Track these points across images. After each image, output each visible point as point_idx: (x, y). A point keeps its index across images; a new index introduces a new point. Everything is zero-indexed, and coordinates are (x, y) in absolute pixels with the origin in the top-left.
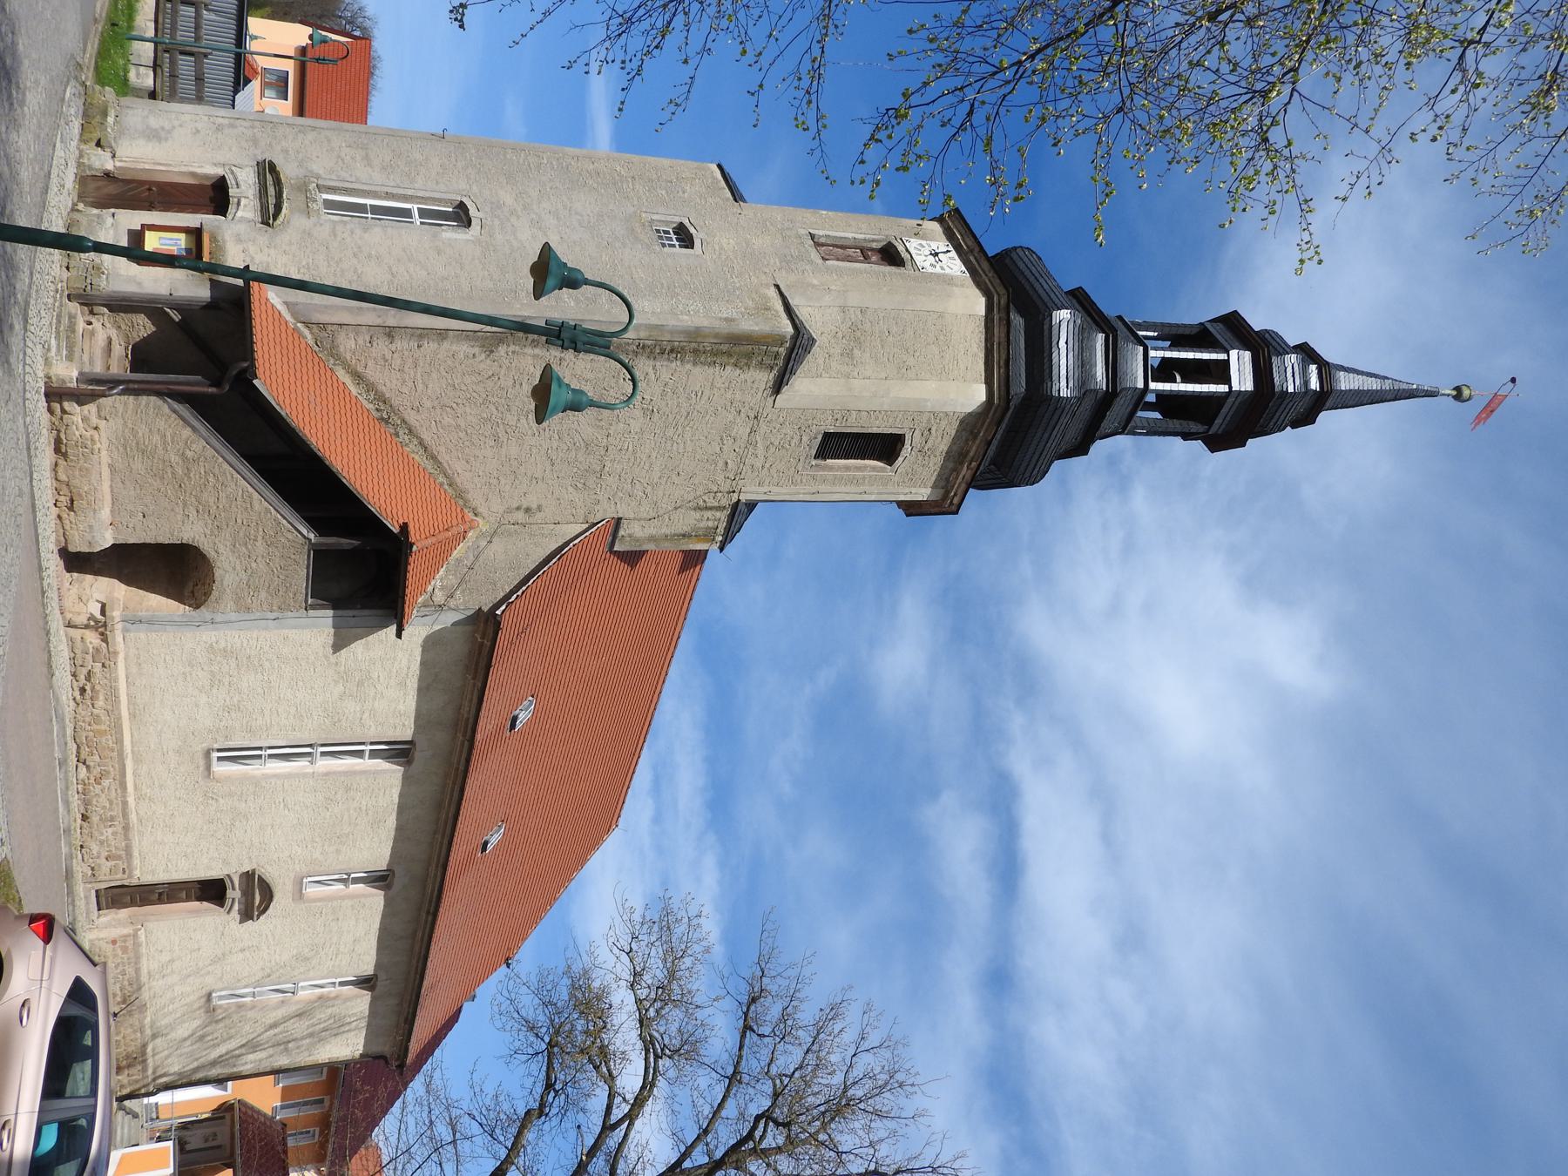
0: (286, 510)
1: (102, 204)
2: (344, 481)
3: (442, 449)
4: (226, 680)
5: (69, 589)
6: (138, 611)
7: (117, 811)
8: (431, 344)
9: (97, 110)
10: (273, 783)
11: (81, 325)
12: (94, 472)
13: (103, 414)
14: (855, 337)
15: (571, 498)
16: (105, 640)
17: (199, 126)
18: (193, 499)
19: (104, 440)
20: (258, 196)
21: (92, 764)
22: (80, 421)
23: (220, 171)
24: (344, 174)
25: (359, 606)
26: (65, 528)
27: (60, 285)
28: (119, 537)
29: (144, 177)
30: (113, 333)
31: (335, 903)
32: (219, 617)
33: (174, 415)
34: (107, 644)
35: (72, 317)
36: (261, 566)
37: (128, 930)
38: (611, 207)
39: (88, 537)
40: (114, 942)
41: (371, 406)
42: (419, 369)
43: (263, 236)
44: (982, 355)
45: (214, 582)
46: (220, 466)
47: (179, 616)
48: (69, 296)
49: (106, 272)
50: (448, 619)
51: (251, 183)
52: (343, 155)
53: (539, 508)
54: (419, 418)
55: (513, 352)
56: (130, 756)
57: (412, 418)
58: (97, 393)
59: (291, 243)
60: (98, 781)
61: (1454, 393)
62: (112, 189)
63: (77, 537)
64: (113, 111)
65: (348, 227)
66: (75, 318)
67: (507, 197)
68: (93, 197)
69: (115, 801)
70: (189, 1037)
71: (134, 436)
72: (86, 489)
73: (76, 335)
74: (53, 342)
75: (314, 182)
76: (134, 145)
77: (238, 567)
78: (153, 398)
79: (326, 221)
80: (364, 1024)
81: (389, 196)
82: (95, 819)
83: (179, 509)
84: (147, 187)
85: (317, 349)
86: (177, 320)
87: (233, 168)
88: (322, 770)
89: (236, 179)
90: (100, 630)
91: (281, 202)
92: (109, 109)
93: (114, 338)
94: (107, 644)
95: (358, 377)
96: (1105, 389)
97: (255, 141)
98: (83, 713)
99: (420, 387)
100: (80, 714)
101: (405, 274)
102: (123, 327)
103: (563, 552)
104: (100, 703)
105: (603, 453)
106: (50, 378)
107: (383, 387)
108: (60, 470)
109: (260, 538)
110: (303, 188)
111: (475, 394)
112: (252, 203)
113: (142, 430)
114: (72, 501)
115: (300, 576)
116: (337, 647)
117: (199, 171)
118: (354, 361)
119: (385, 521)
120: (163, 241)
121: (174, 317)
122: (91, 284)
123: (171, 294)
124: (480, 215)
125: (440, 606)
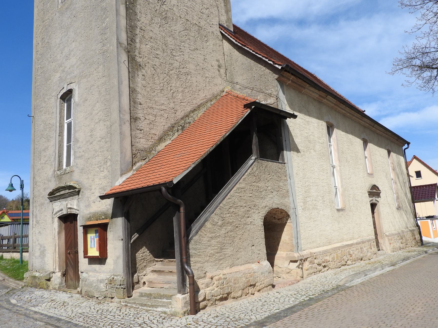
0: (242, 170)
1: (78, 278)
2: (227, 134)
3: (194, 102)
4: (315, 202)
5: (283, 278)
6: (293, 245)
7: (359, 247)
8: (139, 97)
9: (34, 281)
10: (344, 183)
11: (145, 289)
12: (236, 276)
13: (203, 275)
15: (211, 45)
16: (306, 259)
17: (37, 232)
18: (243, 220)
19: (218, 272)
20: (65, 199)
21: (347, 259)
22: (209, 288)
23: (56, 219)
24: (52, 159)
25: (281, 138)
26: (263, 287)
27: (122, 304)
28: (264, 258)
29: (64, 257)
30: (149, 269)
31: (373, 162)
32: (292, 206)
33: (199, 233)
34: (308, 258)
35: (141, 295)
36: (269, 184)
37: (386, 239)
38: (57, 25)
39: (267, 274)
40: (390, 244)
41: (176, 134)
42: (154, 106)
43: (85, 193)
45: (278, 208)
46: (225, 205)
47: (293, 225)
48: (128, 297)
49: (113, 276)
50: (281, 95)
51: (60, 204)
52: (44, 162)
53: (218, 61)
54: (180, 111)
55: (139, 54)
56: (342, 243)
57: (180, 114)
58: (191, 282)
59: (88, 178)
60: (351, 255)
62: (71, 273)
63: (267, 280)
64: (34, 273)
65: (77, 150)
66: (142, 293)
68: (76, 281)
69: (356, 248)
70: (406, 216)
71: (214, 255)
72: (244, 279)
73: (152, 292)
74: (160, 309)
75: (57, 172)
76: (48, 263)
77: (271, 196)
78: (191, 246)
79: (75, 162)
80: (398, 155)
81: (61, 134)
82: (362, 255)
83: (248, 227)
84: (68, 255)
85: (147, 160)
86: (138, 235)
87: (54, 213)
88: (338, 162)
89: (59, 211)
90: (303, 262)
91: (67, 187)
92: (33, 275)
93: (151, 269)
94: (308, 258)
95: (161, 139)
97: (42, 204)
98: (332, 265)
99: (163, 107)
100: (332, 266)
101: (99, 114)
102: (145, 264)
103: (240, 45)
104: (328, 258)
105: (189, 23)
106: (185, 313)
107: (166, 126)
108: (236, 295)
109: (257, 184)
110: (59, 177)
111: (165, 80)
112: (70, 202)
113: (210, 251)
114: (251, 285)
115: (272, 165)
116: (298, 151)
117: (57, 230)
118: (152, 140)
119: (245, 116)
120: (93, 245)
121: (136, 237)
122: (120, 285)
123: (122, 240)
124: (65, 86)
125: (277, 99)
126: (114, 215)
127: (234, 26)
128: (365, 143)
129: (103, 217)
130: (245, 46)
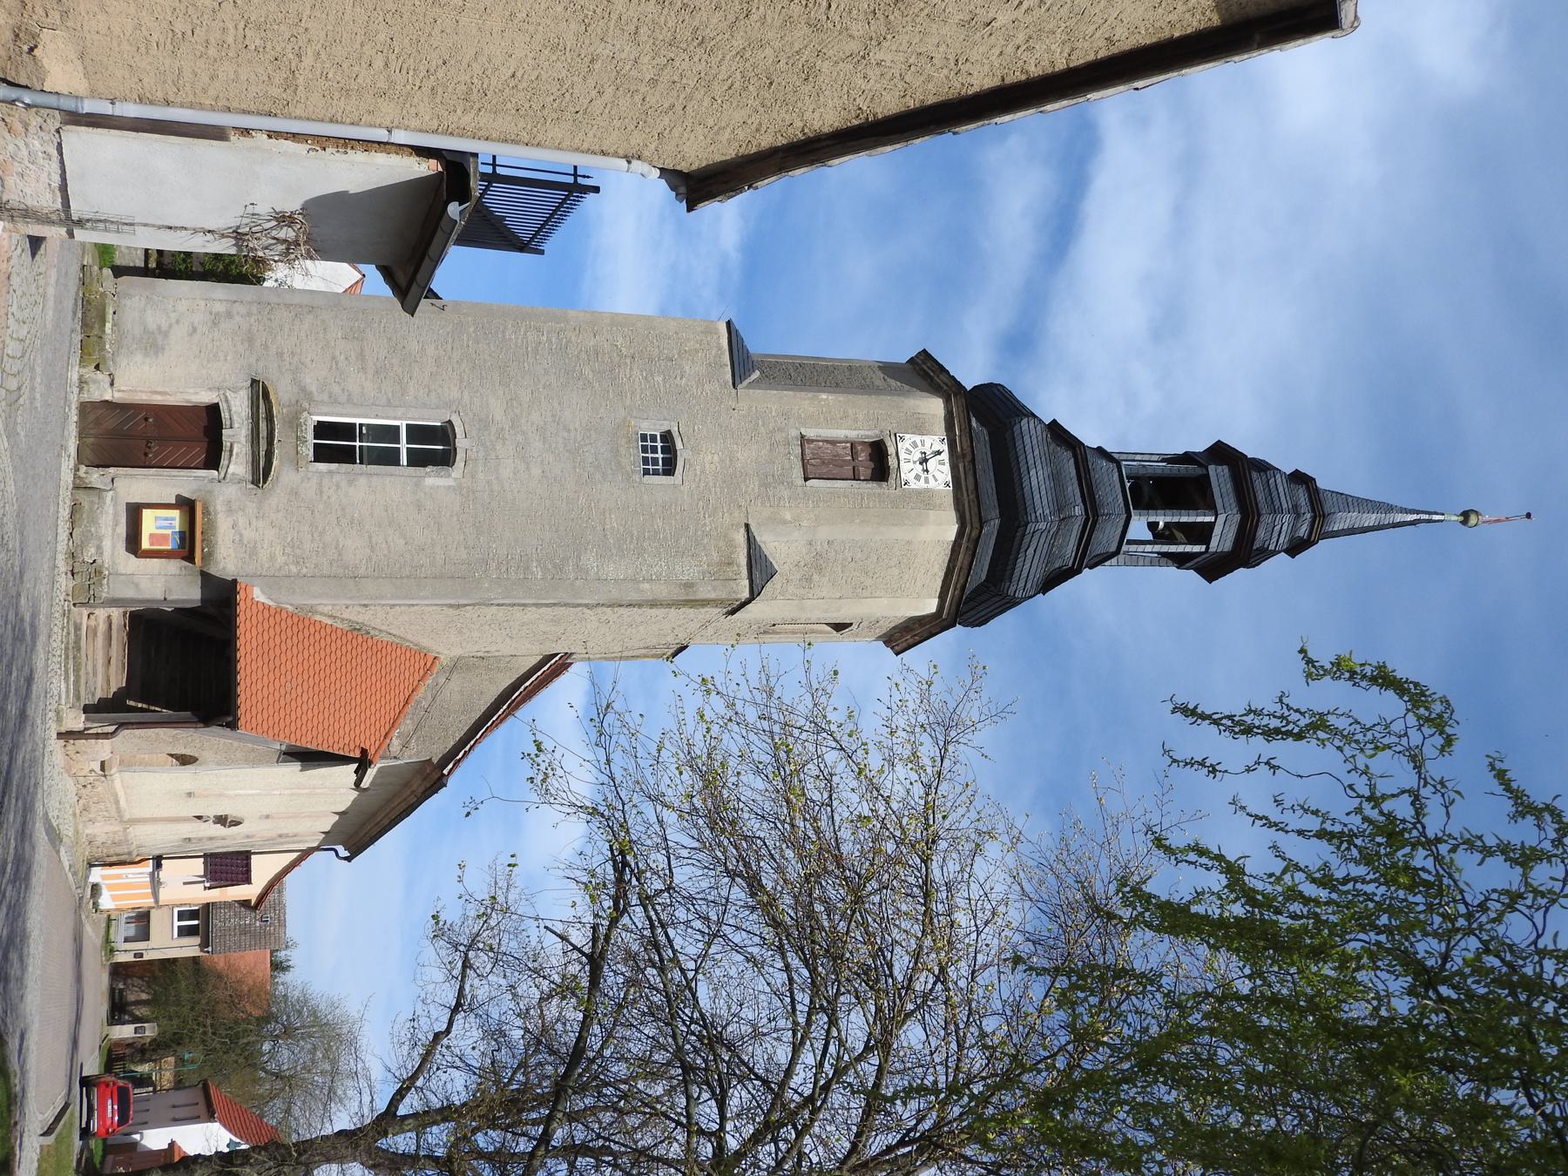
14: (816, 565)
44: (942, 574)
61: (1461, 518)
67: (497, 410)
96: (1070, 565)
126: (206, 578)
127: (571, 664)
128: (340, 814)
129: (206, 550)
130: (508, 707)
